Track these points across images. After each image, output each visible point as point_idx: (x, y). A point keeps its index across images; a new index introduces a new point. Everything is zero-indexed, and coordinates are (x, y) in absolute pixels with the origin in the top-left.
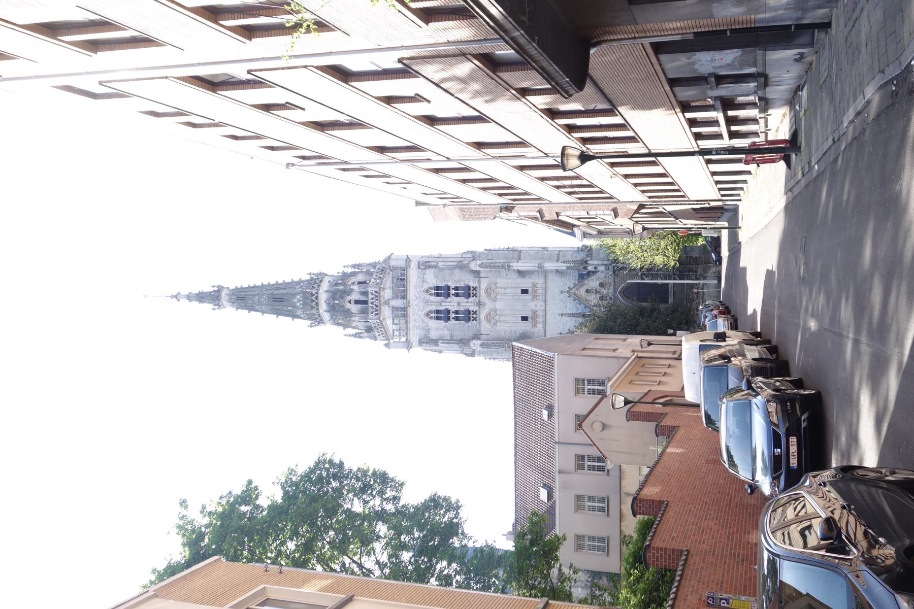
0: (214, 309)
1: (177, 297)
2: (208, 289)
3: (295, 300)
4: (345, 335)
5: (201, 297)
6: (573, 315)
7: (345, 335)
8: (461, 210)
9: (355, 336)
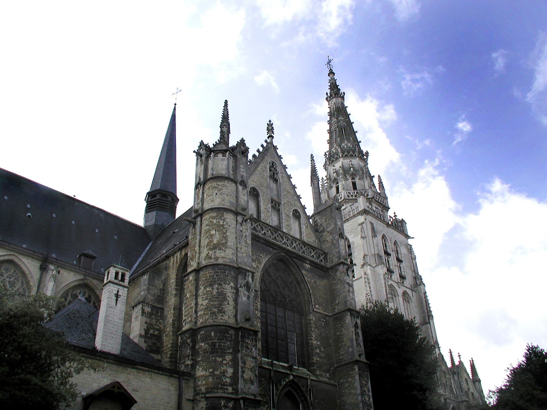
0: (327, 94)
3: (346, 143)
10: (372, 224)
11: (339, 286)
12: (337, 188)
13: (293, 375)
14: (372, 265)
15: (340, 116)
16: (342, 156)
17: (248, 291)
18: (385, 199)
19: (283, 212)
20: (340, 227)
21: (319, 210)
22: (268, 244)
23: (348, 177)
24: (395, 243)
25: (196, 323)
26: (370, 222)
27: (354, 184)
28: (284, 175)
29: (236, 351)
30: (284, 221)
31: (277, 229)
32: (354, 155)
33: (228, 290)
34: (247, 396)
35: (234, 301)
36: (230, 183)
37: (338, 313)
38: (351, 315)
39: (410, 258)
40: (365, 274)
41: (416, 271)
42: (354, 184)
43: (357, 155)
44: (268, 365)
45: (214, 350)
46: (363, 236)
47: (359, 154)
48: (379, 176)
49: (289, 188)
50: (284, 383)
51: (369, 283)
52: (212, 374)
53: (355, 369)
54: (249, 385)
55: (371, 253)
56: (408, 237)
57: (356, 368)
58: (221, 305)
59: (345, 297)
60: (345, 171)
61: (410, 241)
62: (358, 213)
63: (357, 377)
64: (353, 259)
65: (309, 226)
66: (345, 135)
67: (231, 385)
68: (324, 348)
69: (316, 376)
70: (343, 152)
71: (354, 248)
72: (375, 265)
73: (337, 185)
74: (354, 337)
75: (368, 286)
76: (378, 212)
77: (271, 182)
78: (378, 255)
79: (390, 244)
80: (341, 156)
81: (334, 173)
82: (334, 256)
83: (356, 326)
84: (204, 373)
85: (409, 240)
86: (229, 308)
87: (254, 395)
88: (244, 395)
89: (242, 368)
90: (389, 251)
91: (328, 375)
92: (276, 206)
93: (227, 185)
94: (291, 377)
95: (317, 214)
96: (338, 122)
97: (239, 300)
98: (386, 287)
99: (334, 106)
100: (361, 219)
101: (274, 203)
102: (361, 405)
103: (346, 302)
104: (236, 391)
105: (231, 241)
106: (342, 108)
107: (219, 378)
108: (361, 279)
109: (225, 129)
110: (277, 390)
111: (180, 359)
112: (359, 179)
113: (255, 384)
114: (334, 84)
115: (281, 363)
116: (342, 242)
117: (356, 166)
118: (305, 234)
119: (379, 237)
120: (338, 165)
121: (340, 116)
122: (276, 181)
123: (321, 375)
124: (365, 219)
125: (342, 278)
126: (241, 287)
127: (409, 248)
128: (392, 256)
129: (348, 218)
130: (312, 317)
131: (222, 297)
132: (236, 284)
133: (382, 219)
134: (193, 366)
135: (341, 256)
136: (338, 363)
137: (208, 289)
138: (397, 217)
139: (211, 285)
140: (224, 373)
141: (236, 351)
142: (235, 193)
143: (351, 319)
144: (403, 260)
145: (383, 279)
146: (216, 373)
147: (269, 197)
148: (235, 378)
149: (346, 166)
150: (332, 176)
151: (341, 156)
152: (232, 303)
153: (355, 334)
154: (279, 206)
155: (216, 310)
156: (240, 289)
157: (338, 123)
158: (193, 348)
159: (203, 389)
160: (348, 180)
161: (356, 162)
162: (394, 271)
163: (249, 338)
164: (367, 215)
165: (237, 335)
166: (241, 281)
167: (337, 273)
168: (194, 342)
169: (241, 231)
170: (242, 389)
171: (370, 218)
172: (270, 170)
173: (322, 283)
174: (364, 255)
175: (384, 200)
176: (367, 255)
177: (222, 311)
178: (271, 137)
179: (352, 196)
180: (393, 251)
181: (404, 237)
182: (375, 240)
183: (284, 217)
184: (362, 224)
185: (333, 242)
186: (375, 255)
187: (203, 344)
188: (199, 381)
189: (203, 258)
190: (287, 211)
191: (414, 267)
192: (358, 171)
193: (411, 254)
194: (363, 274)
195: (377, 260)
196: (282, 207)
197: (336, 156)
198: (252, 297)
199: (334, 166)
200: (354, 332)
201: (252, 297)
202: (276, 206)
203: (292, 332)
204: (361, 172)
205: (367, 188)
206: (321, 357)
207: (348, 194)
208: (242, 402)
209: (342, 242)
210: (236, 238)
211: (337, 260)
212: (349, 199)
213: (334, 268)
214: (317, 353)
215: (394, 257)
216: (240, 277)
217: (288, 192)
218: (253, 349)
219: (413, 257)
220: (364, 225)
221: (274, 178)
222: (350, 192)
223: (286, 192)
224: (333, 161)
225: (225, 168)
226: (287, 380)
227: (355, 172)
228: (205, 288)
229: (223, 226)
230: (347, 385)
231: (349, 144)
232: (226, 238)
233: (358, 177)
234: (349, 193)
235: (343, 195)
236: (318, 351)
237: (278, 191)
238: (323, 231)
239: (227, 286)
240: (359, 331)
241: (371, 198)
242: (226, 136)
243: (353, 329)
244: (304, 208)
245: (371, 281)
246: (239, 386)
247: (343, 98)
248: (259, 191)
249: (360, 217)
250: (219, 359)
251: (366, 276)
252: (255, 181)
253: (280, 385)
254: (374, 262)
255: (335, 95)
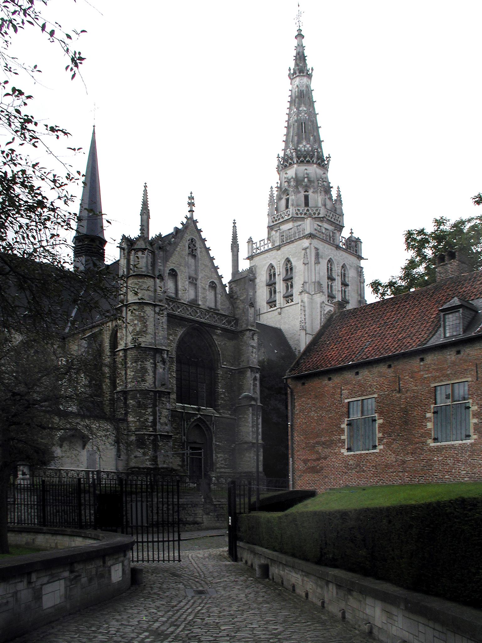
0: (290, 70)
1: (300, 36)
2: (310, 63)
3: (304, 143)
4: (272, 188)
5: (301, 58)
6: (455, 637)
7: (272, 188)
8: (356, 252)
9: (271, 196)
10: (317, 249)
11: (244, 348)
12: (287, 200)
13: (201, 415)
14: (310, 292)
15: (303, 105)
16: (297, 161)
17: (164, 365)
18: (340, 216)
19: (200, 286)
20: (251, 296)
21: (235, 279)
22: (182, 319)
23: (300, 189)
24: (344, 266)
25: (126, 386)
26: (315, 248)
27: (306, 198)
28: (203, 249)
29: (155, 406)
30: (200, 294)
31: (193, 304)
32: (311, 161)
33: (149, 365)
34: (163, 433)
35: (153, 372)
36: (149, 279)
37: (242, 368)
38: (251, 371)
39: (359, 281)
40: (302, 301)
41: (362, 295)
42: (306, 198)
43: (315, 161)
44: (181, 409)
45: (140, 405)
46: (306, 262)
47: (318, 159)
48: (338, 188)
49: (207, 262)
50: (192, 420)
51: (305, 311)
52: (139, 420)
53: (249, 410)
54: (164, 426)
55: (311, 280)
56: (360, 258)
57: (251, 409)
58: (143, 376)
59: (248, 357)
60: (298, 181)
61: (363, 263)
62: (303, 236)
63: (251, 415)
64: (293, 283)
65: (224, 294)
66: (305, 132)
67: (151, 427)
68: (228, 393)
69: (220, 413)
70: (298, 157)
71: (295, 272)
72: (313, 293)
73: (288, 196)
74: (252, 388)
75: (303, 313)
76: (328, 234)
77: (190, 257)
78: (319, 282)
79: (336, 269)
80: (295, 162)
81: (285, 182)
82: (243, 322)
83: (255, 379)
84: (133, 419)
85: (362, 261)
86: (149, 378)
87: (167, 432)
88: (160, 433)
89: (159, 417)
90: (334, 275)
91: (230, 412)
92: (193, 281)
93: (147, 281)
94: (199, 416)
95: (233, 281)
96: (299, 112)
97: (157, 372)
98: (321, 315)
99: (297, 90)
100: (306, 243)
101: (191, 279)
102: (251, 434)
103: (248, 361)
104: (155, 430)
105: (150, 329)
106: (306, 92)
107: (143, 422)
108: (298, 305)
109: (145, 217)
110: (187, 425)
111: (117, 409)
112: (313, 192)
113: (168, 425)
114: (301, 54)
115: (192, 406)
116: (251, 311)
117: (312, 176)
118: (219, 303)
119: (324, 263)
120: (291, 172)
121: (303, 105)
122: (194, 256)
123: (224, 413)
124: (310, 244)
125: (247, 342)
126: (158, 362)
127: (360, 271)
128: (336, 280)
129: (293, 239)
130: (220, 372)
131: (144, 370)
132: (155, 361)
133: (331, 240)
134: (126, 414)
135: (249, 323)
136: (238, 404)
137: (134, 364)
138: (353, 235)
139: (136, 362)
140: (146, 420)
141: (155, 406)
142: (153, 287)
143: (251, 374)
144: (350, 284)
145: (319, 308)
146: (141, 419)
147: (187, 274)
148: (154, 423)
149: (300, 175)
150: (283, 185)
151: (295, 162)
152: (151, 374)
153: (254, 385)
154: (196, 280)
155: (140, 379)
156: (157, 364)
157: (298, 116)
158: (125, 403)
159: (133, 429)
160: (299, 192)
161: (313, 170)
162: (336, 297)
163: (164, 397)
164: (313, 239)
165: (155, 395)
166: (158, 358)
167: (244, 337)
168: (126, 399)
169: (158, 319)
170: (159, 429)
171: (316, 243)
172: (189, 248)
173: (230, 344)
174: (304, 282)
175: (338, 218)
176: (306, 283)
177: (144, 380)
178: (191, 211)
179: (301, 214)
180: (338, 275)
181: (356, 259)
182: (317, 267)
183: (200, 291)
184: (305, 249)
185: (243, 310)
186: (315, 282)
187: (132, 401)
188: (130, 423)
189: (130, 341)
190: (203, 283)
191: (361, 291)
192: (313, 182)
193: (361, 278)
194: (300, 301)
195: (316, 288)
196: (199, 282)
197: (290, 161)
198: (166, 368)
199: (286, 173)
200: (252, 384)
201: (166, 368)
202: (193, 281)
203: (202, 383)
204: (316, 183)
205: (320, 205)
206: (225, 401)
207: (297, 211)
208: (159, 436)
209: (251, 311)
210: (154, 325)
211: (245, 326)
212: (298, 217)
213: (242, 332)
214: (221, 398)
215: (338, 282)
216: (158, 355)
217: (206, 266)
218: (168, 404)
219: (362, 281)
220: (308, 250)
221: (193, 254)
222: (299, 208)
223: (204, 266)
224: (286, 166)
225: (145, 265)
226: (195, 418)
227: (309, 184)
228: (132, 364)
229: (143, 317)
230: (244, 419)
231: (308, 146)
232: (146, 326)
233: (312, 190)
234: (299, 210)
235: (291, 211)
236: (223, 396)
237: (196, 266)
238: (237, 298)
239: (148, 363)
240: (258, 383)
241: (322, 218)
242: (146, 229)
243: (252, 382)
244: (221, 277)
245: (306, 309)
246: (157, 427)
247: (309, 76)
248: (177, 271)
249: (305, 240)
250: (144, 411)
251: (302, 304)
252: (174, 262)
253: (190, 421)
254: (313, 289)
255: (300, 73)
